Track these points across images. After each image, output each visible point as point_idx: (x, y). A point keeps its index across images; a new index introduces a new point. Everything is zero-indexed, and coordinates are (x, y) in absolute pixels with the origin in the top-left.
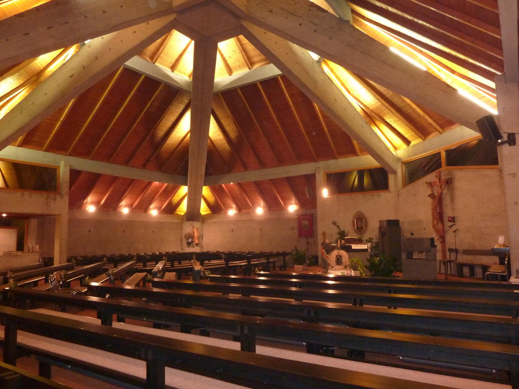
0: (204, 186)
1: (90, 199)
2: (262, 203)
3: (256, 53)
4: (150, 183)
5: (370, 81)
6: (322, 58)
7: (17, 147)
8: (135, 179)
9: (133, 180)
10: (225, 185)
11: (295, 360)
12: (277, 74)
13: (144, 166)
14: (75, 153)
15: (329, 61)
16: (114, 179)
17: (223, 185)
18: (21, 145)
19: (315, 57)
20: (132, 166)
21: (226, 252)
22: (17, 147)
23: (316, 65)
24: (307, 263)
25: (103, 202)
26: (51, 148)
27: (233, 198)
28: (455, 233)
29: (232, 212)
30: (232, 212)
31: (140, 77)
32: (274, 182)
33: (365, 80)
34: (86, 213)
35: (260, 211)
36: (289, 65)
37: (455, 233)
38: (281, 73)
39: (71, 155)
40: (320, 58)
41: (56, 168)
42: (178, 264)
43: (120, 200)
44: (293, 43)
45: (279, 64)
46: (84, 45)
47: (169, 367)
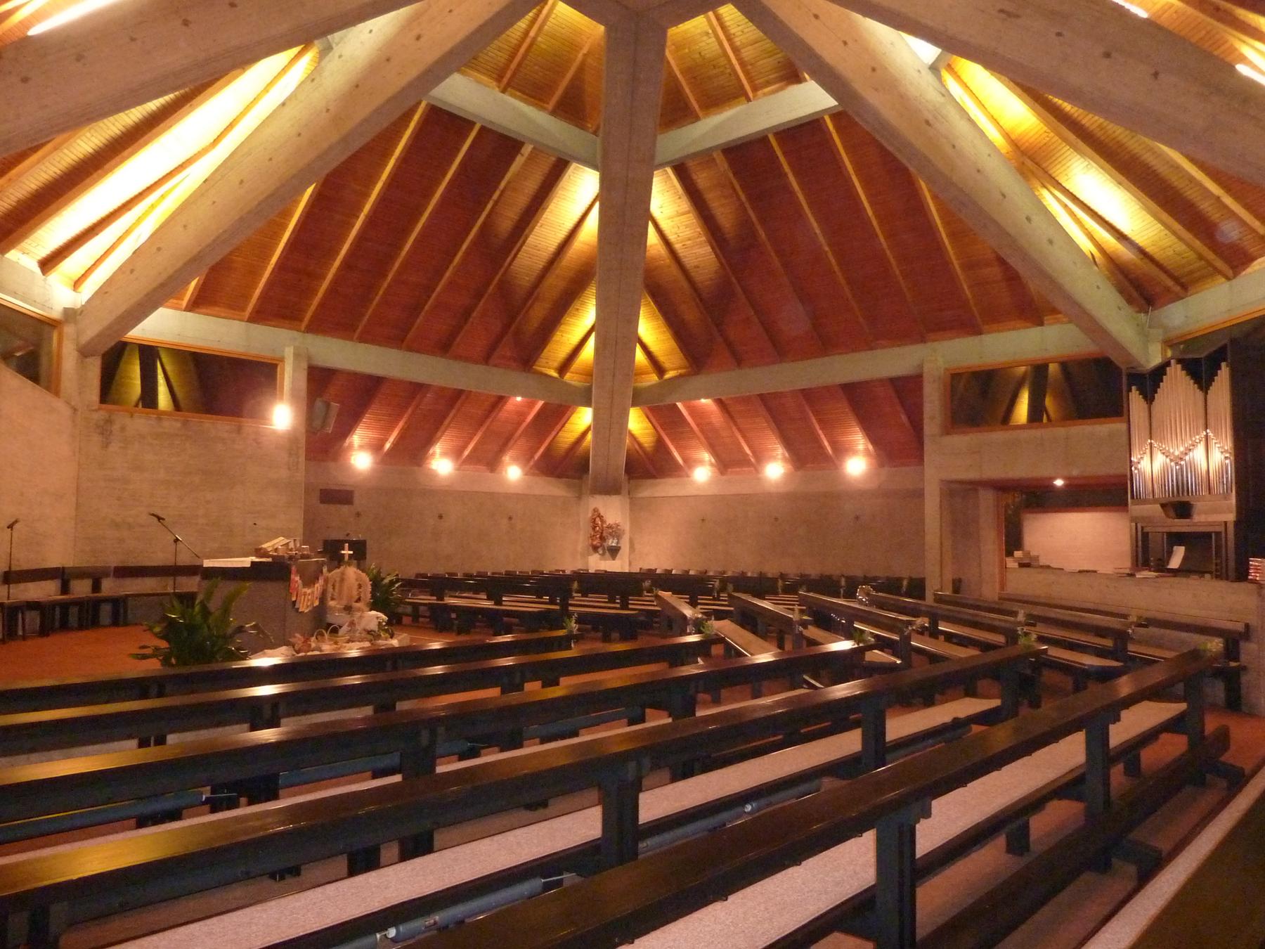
0: (634, 405)
1: (358, 437)
2: (780, 451)
3: (1146, 232)
4: (501, 400)
5: (1056, 100)
6: (946, 53)
7: (184, 311)
8: (464, 391)
9: (459, 393)
10: (685, 406)
11: (947, 795)
12: (819, 108)
13: (486, 358)
14: (319, 326)
15: (959, 58)
16: (417, 389)
17: (679, 405)
18: (197, 304)
19: (927, 52)
20: (458, 357)
21: (528, 573)
22: (185, 312)
23: (929, 78)
24: (455, 628)
25: (388, 446)
26: (260, 316)
27: (707, 438)
28: (12, 530)
29: (703, 473)
30: (703, 473)
31: (471, 129)
32: (810, 396)
33: (1050, 101)
34: (348, 468)
35: (775, 470)
36: (860, 86)
37: (12, 530)
38: (836, 103)
39: (363, 339)
40: (941, 53)
41: (274, 362)
42: (582, 596)
43: (429, 441)
44: (865, 14)
45: (831, 80)
46: (330, 52)
47: (604, 814)
